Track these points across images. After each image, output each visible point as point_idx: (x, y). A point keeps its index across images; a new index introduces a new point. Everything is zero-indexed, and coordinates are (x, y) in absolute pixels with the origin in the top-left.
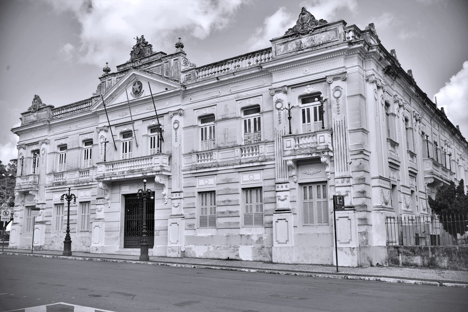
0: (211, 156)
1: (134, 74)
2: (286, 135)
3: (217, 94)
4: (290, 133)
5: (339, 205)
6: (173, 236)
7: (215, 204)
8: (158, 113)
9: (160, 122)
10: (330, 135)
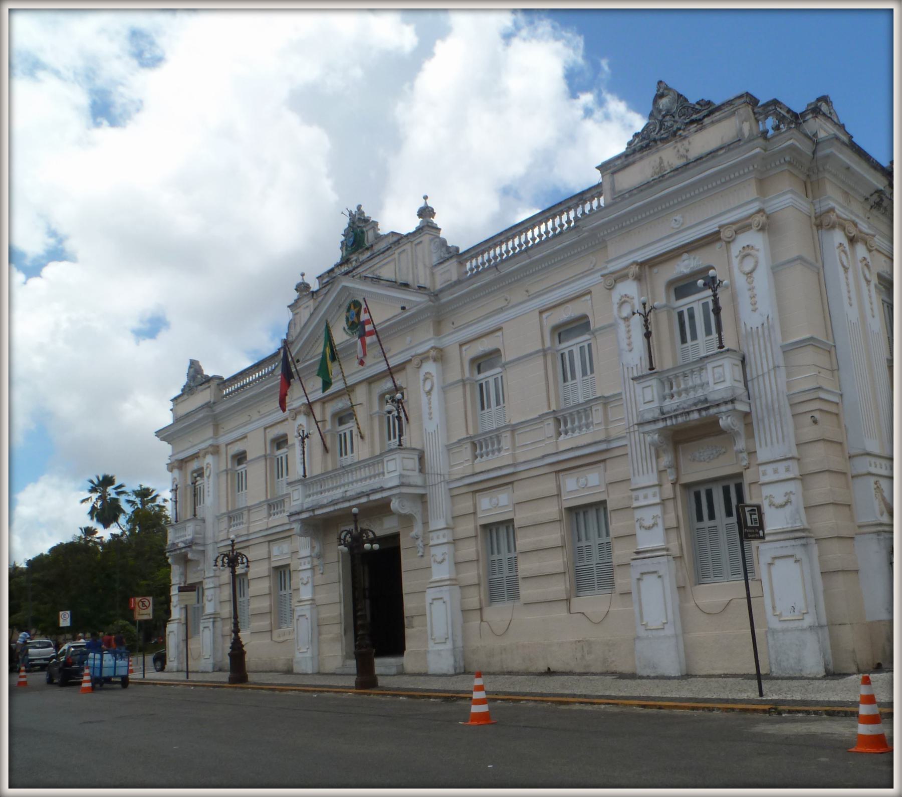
0: (587, 417)
1: (344, 287)
2: (644, 373)
3: (502, 303)
4: (651, 368)
5: (750, 528)
6: (437, 626)
7: (608, 534)
8: (393, 362)
9: (398, 383)
10: (739, 363)
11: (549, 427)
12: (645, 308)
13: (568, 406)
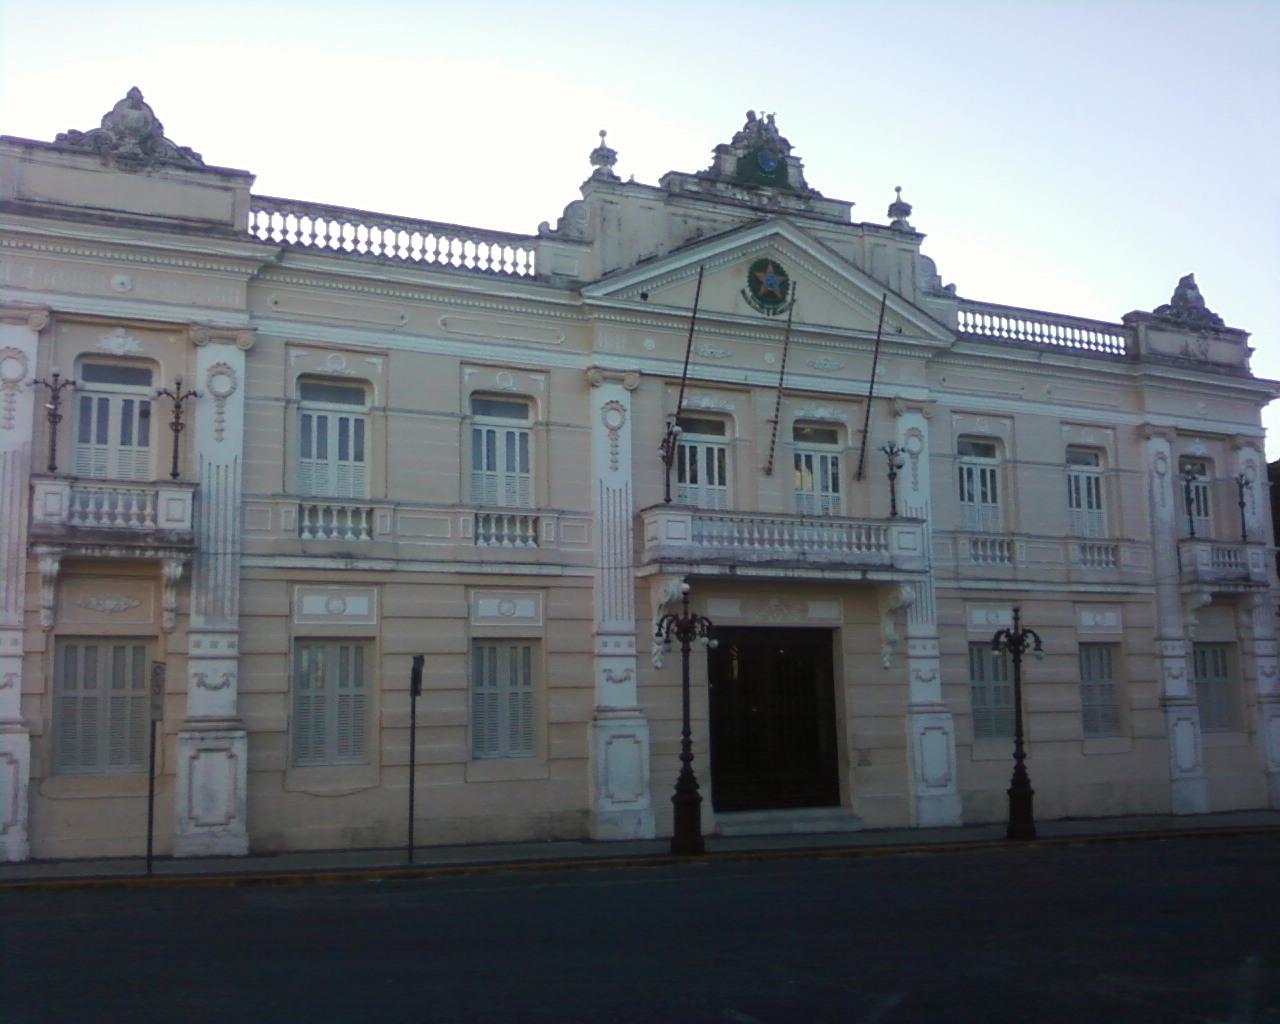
11: (466, 523)
12: (178, 389)
13: (343, 494)
